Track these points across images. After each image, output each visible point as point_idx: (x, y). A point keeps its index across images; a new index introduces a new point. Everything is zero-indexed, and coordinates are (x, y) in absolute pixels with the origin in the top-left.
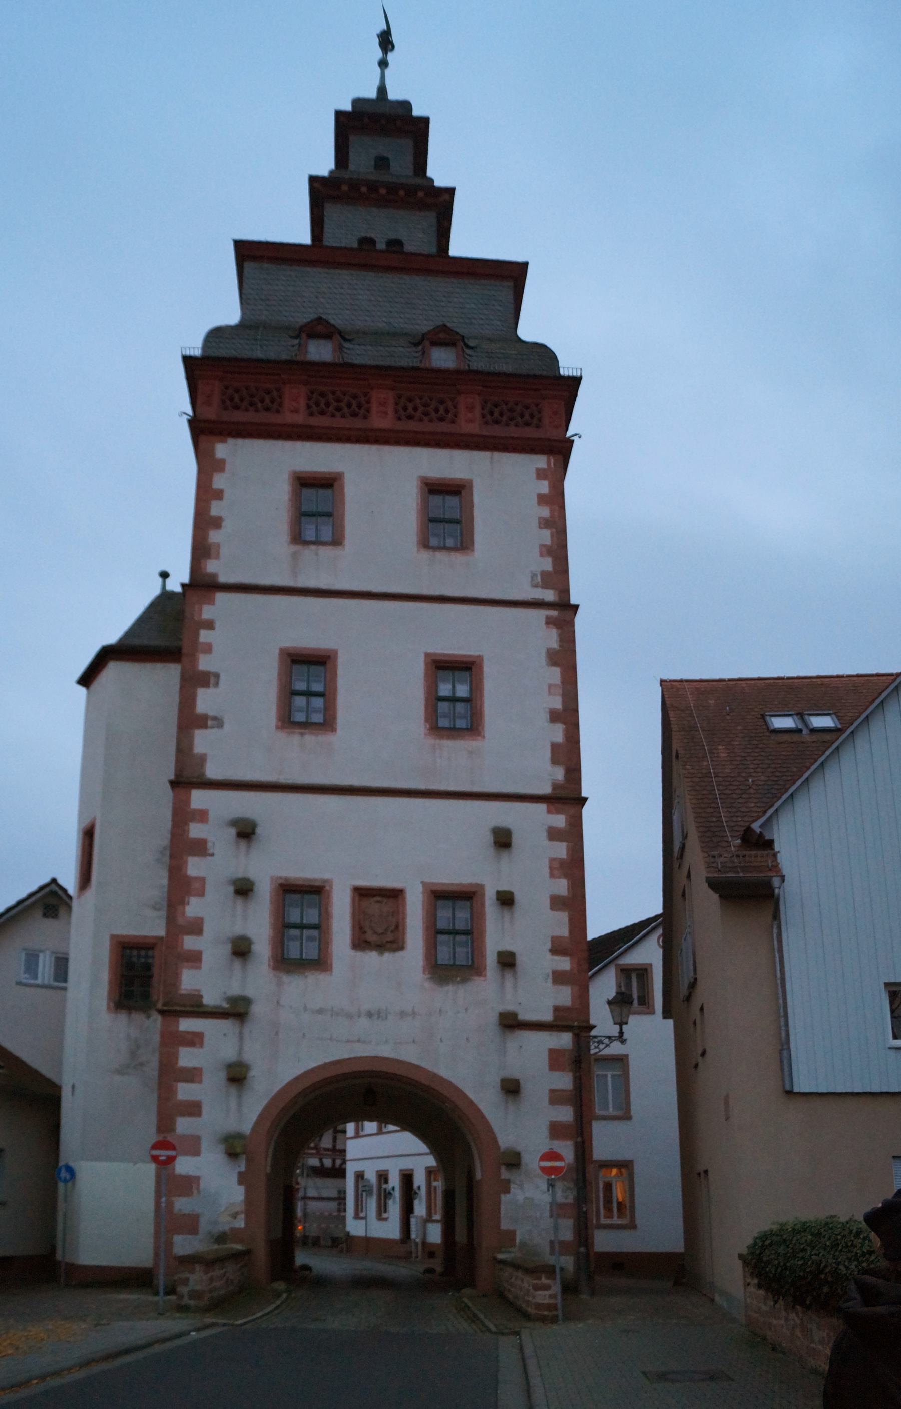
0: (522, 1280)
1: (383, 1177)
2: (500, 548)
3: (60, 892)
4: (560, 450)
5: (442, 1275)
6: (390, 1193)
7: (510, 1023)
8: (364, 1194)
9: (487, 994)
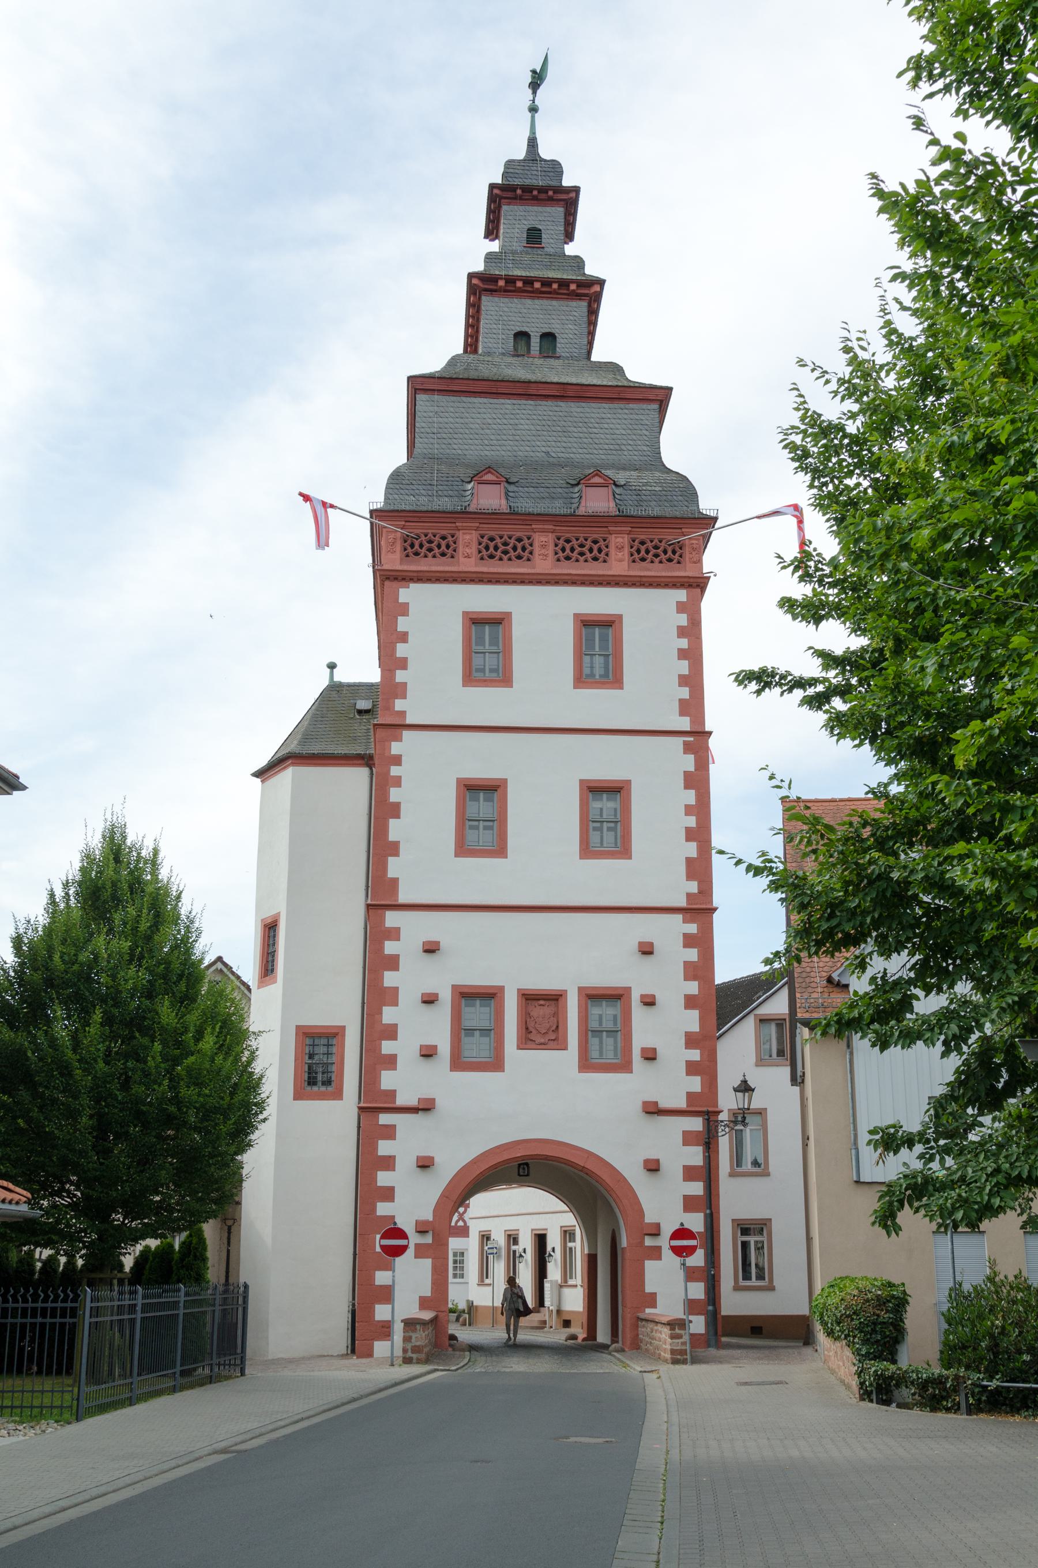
0: (661, 1332)
1: (513, 1238)
2: (647, 690)
3: (225, 970)
4: (698, 584)
5: (584, 1340)
6: (521, 1256)
7: (653, 1110)
8: (491, 1257)
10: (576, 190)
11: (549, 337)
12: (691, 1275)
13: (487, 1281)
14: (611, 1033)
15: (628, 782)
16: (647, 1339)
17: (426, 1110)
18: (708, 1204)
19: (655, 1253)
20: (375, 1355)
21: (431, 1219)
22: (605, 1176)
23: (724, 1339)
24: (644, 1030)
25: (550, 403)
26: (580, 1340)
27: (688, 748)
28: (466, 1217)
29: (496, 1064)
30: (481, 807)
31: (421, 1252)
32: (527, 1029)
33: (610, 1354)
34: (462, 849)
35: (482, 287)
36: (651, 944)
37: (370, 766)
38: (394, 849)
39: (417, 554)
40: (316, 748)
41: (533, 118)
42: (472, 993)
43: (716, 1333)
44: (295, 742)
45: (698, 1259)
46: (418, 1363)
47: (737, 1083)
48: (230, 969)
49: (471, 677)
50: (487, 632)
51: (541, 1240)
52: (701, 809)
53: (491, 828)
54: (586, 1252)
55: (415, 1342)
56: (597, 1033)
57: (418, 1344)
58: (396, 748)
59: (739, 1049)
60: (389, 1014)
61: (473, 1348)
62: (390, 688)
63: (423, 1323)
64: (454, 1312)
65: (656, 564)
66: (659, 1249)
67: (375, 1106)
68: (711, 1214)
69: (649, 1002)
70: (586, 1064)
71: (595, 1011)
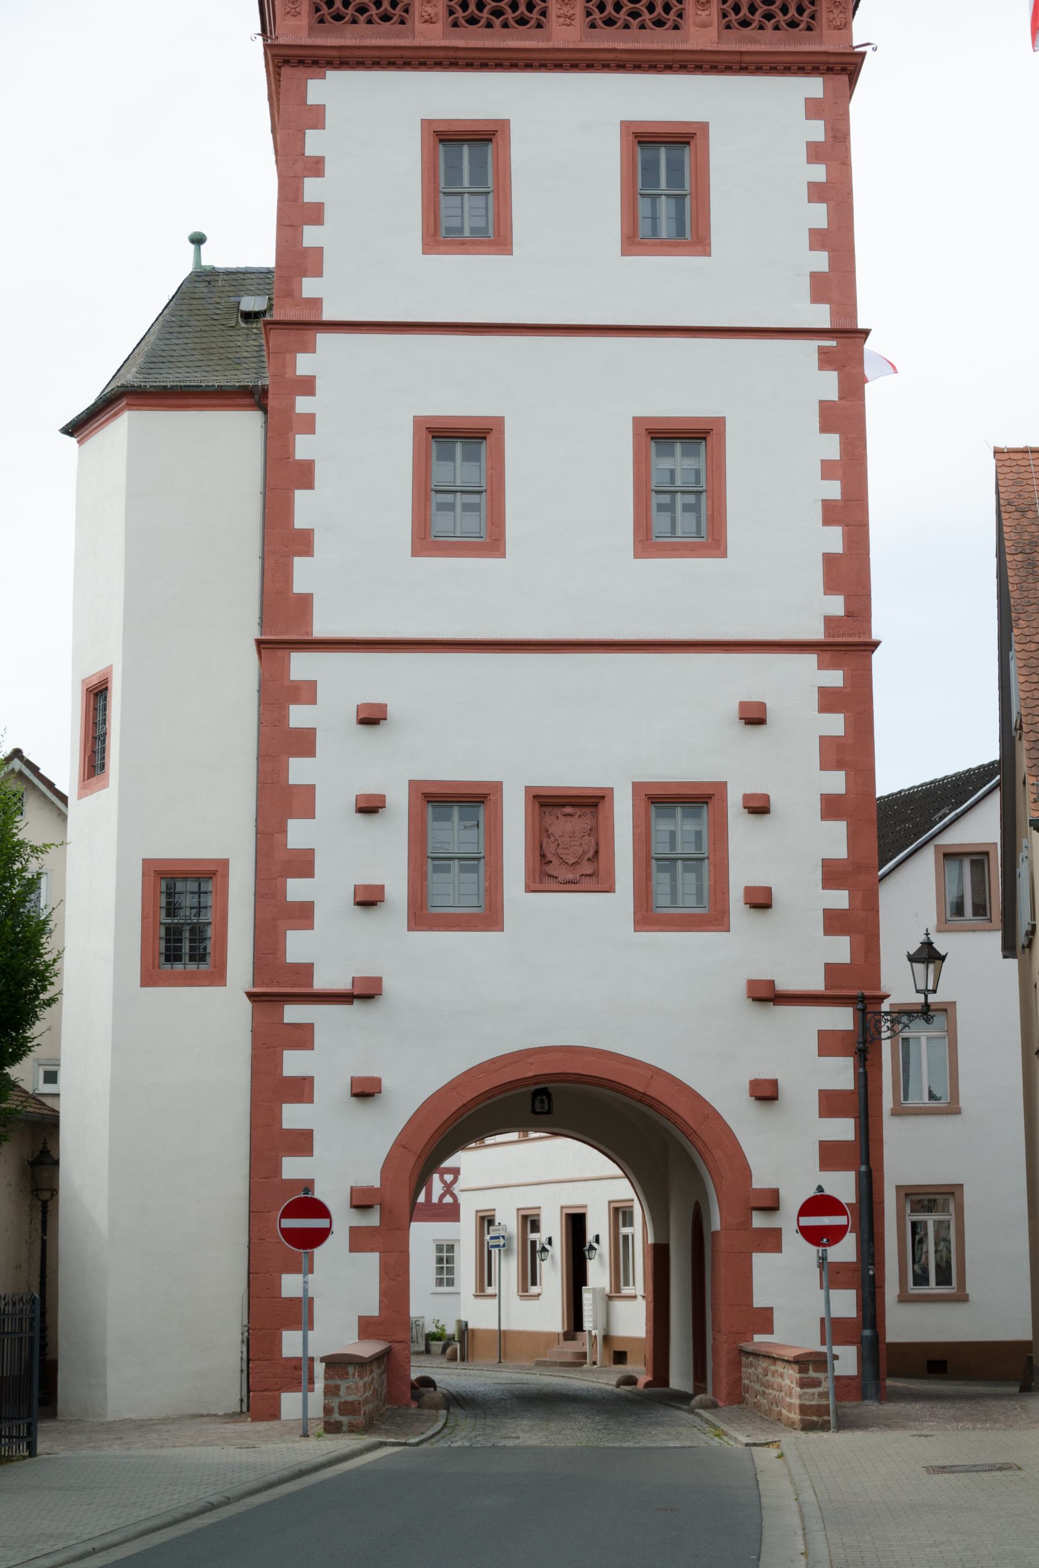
0: (782, 1376)
1: (531, 1222)
3: (27, 772)
4: (845, 67)
5: (648, 1385)
6: (544, 1249)
7: (766, 995)
8: (495, 1252)
12: (833, 1276)
13: (490, 1290)
14: (694, 862)
15: (721, 421)
16: (757, 1387)
17: (367, 997)
18: (864, 1155)
19: (772, 1241)
20: (283, 1417)
21: (377, 1184)
22: (681, 1108)
23: (889, 1382)
24: (751, 855)
26: (640, 1386)
27: (826, 359)
28: (456, 1189)
29: (489, 917)
30: (458, 470)
31: (359, 1241)
32: (543, 856)
33: (691, 1411)
36: (762, 706)
37: (264, 408)
39: (338, 17)
40: (169, 378)
42: (444, 795)
43: (877, 1376)
44: (134, 370)
45: (845, 1250)
46: (351, 1431)
47: (914, 947)
48: (34, 769)
49: (439, 236)
50: (466, 151)
51: (576, 1223)
52: (851, 468)
53: (476, 508)
54: (651, 1240)
55: (345, 1396)
56: (669, 863)
57: (350, 1398)
58: (304, 364)
59: (911, 897)
60: (298, 834)
61: (457, 1401)
62: (296, 259)
63: (360, 1363)
64: (439, 1339)
65: (769, 31)
66: (777, 1233)
67: (279, 989)
68: (869, 1174)
69: (758, 807)
70: (647, 917)
71: (662, 827)
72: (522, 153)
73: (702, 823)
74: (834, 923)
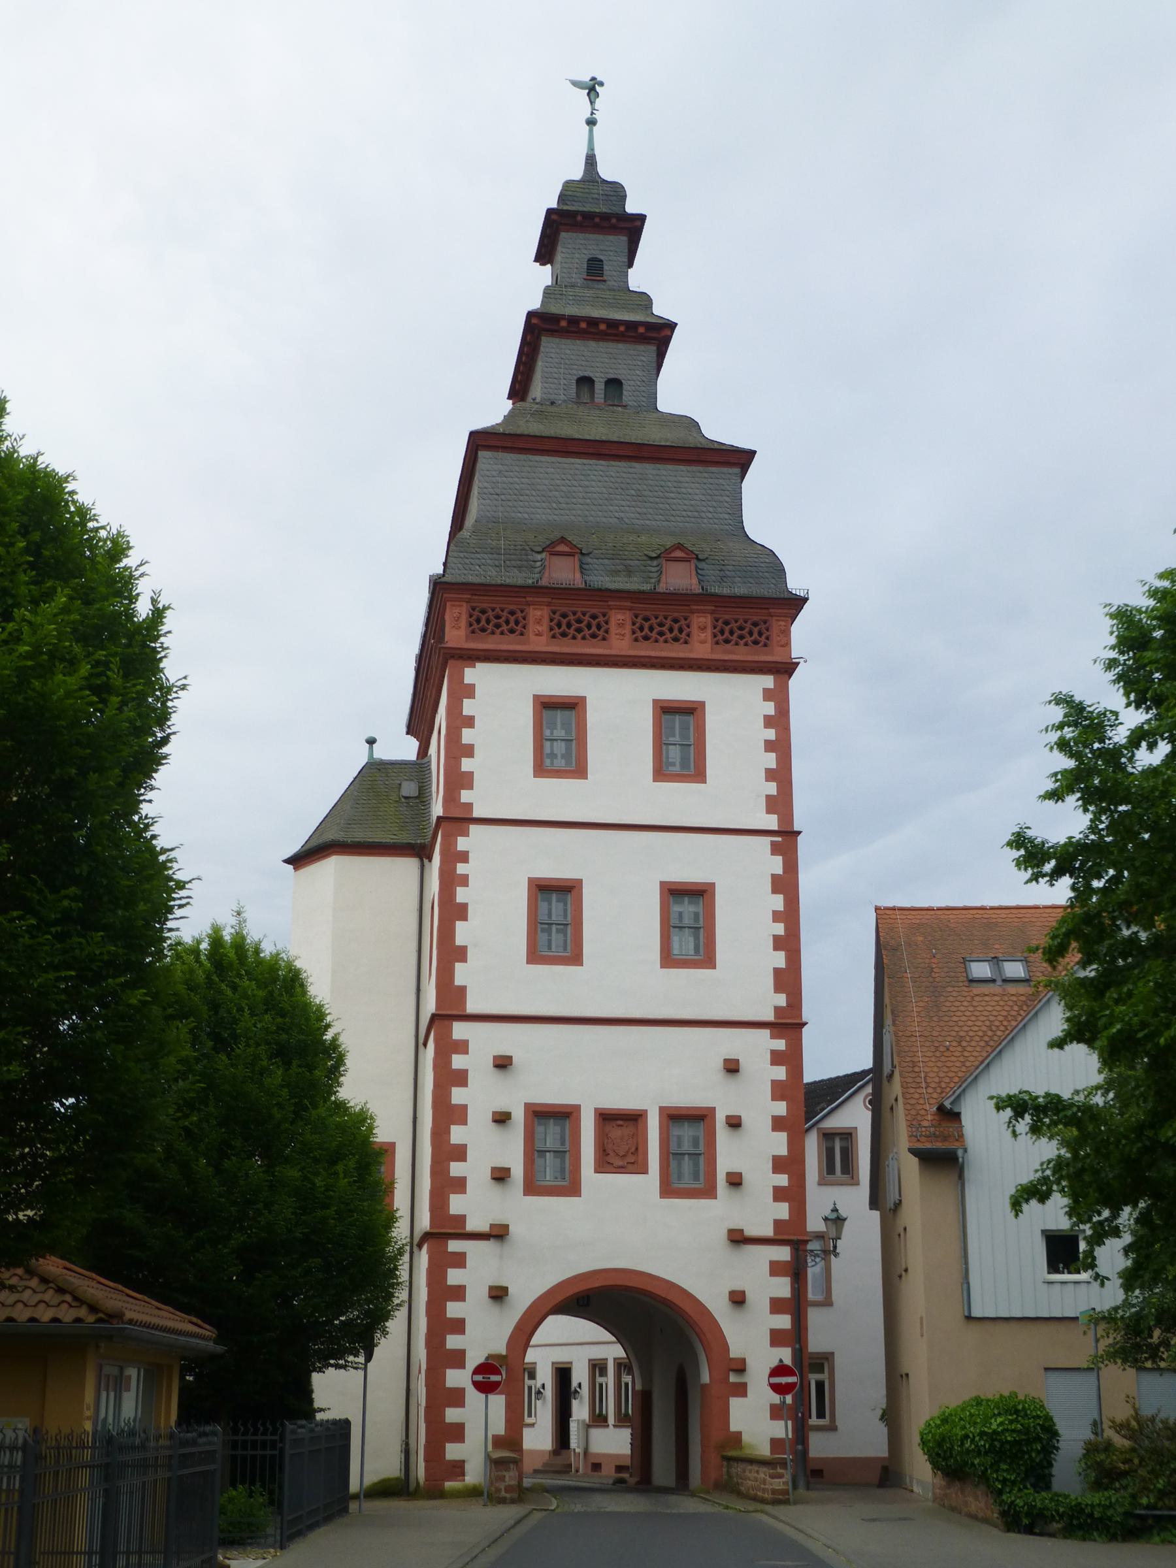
2: (734, 779)
4: (785, 669)
7: (738, 1239)
9: (719, 1213)
10: (642, 218)
11: (614, 384)
14: (694, 1156)
24: (729, 1154)
25: (623, 464)
27: (776, 849)
29: (572, 1188)
34: (534, 956)
35: (539, 327)
38: (461, 954)
39: (483, 630)
41: (591, 131)
50: (559, 720)
51: (563, 1374)
54: (638, 1387)
60: (457, 1134)
69: (734, 1123)
70: (668, 1190)
72: (593, 716)
73: (700, 1130)
74: (779, 1194)
